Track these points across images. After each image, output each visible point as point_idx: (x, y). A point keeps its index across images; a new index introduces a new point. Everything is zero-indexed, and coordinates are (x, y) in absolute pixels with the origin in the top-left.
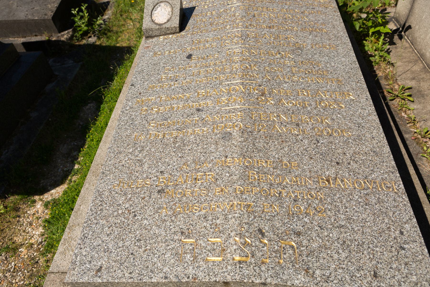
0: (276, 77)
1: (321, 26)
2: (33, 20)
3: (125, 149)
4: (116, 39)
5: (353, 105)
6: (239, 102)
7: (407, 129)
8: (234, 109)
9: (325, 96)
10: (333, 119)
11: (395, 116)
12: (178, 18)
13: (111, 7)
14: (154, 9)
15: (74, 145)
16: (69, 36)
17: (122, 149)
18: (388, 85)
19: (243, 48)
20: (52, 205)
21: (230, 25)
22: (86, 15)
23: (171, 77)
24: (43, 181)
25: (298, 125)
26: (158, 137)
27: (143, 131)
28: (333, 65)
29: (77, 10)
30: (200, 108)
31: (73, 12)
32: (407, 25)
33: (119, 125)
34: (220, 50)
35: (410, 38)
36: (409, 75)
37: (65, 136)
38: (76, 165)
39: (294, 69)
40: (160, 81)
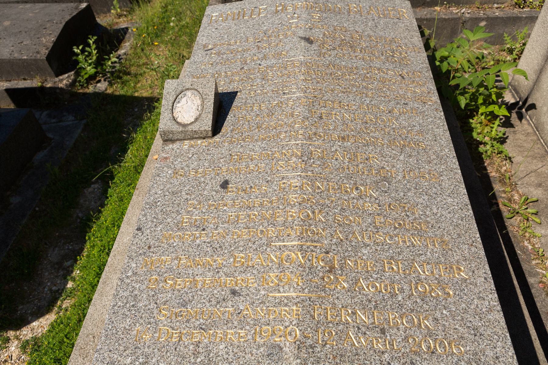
0: (351, 235)
1: (417, 137)
2: (20, 60)
3: (121, 355)
4: (135, 87)
5: (466, 290)
6: (295, 286)
7: (531, 269)
8: (287, 298)
9: (424, 272)
10: (436, 319)
11: (515, 245)
12: (211, 116)
13: (130, 38)
14: (177, 100)
15: (68, 249)
16: (70, 81)
17: (116, 356)
18: (505, 192)
19: (304, 178)
20: (32, 348)
21: (286, 132)
22: (95, 52)
23: (196, 220)
24: (22, 307)
25: (383, 331)
26: (172, 338)
27: (150, 323)
28: (435, 211)
29: (81, 47)
30: (237, 288)
31: (76, 50)
32: (530, 102)
33: (114, 306)
34: (269, 179)
35: (533, 120)
36: (533, 178)
37: (57, 234)
38: (69, 282)
39: (379, 220)
40: (179, 227)
